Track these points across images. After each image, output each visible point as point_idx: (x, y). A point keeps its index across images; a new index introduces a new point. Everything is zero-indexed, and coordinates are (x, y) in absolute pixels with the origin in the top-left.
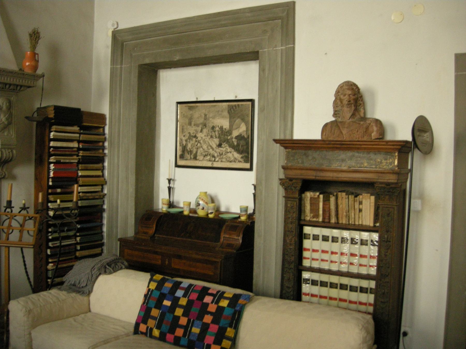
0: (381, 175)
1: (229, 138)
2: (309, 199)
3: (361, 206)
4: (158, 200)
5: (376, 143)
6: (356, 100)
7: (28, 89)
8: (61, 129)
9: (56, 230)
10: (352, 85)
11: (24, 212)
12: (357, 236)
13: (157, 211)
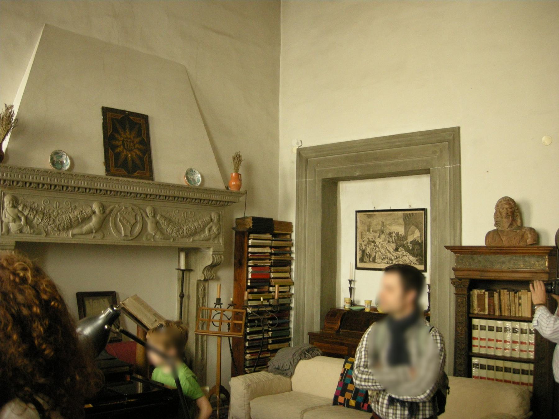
0: (536, 274)
1: (405, 242)
2: (476, 296)
3: (520, 301)
4: (340, 299)
5: (529, 248)
6: (513, 213)
7: (234, 203)
8: (257, 237)
10: (508, 200)
12: (517, 326)
13: (339, 308)
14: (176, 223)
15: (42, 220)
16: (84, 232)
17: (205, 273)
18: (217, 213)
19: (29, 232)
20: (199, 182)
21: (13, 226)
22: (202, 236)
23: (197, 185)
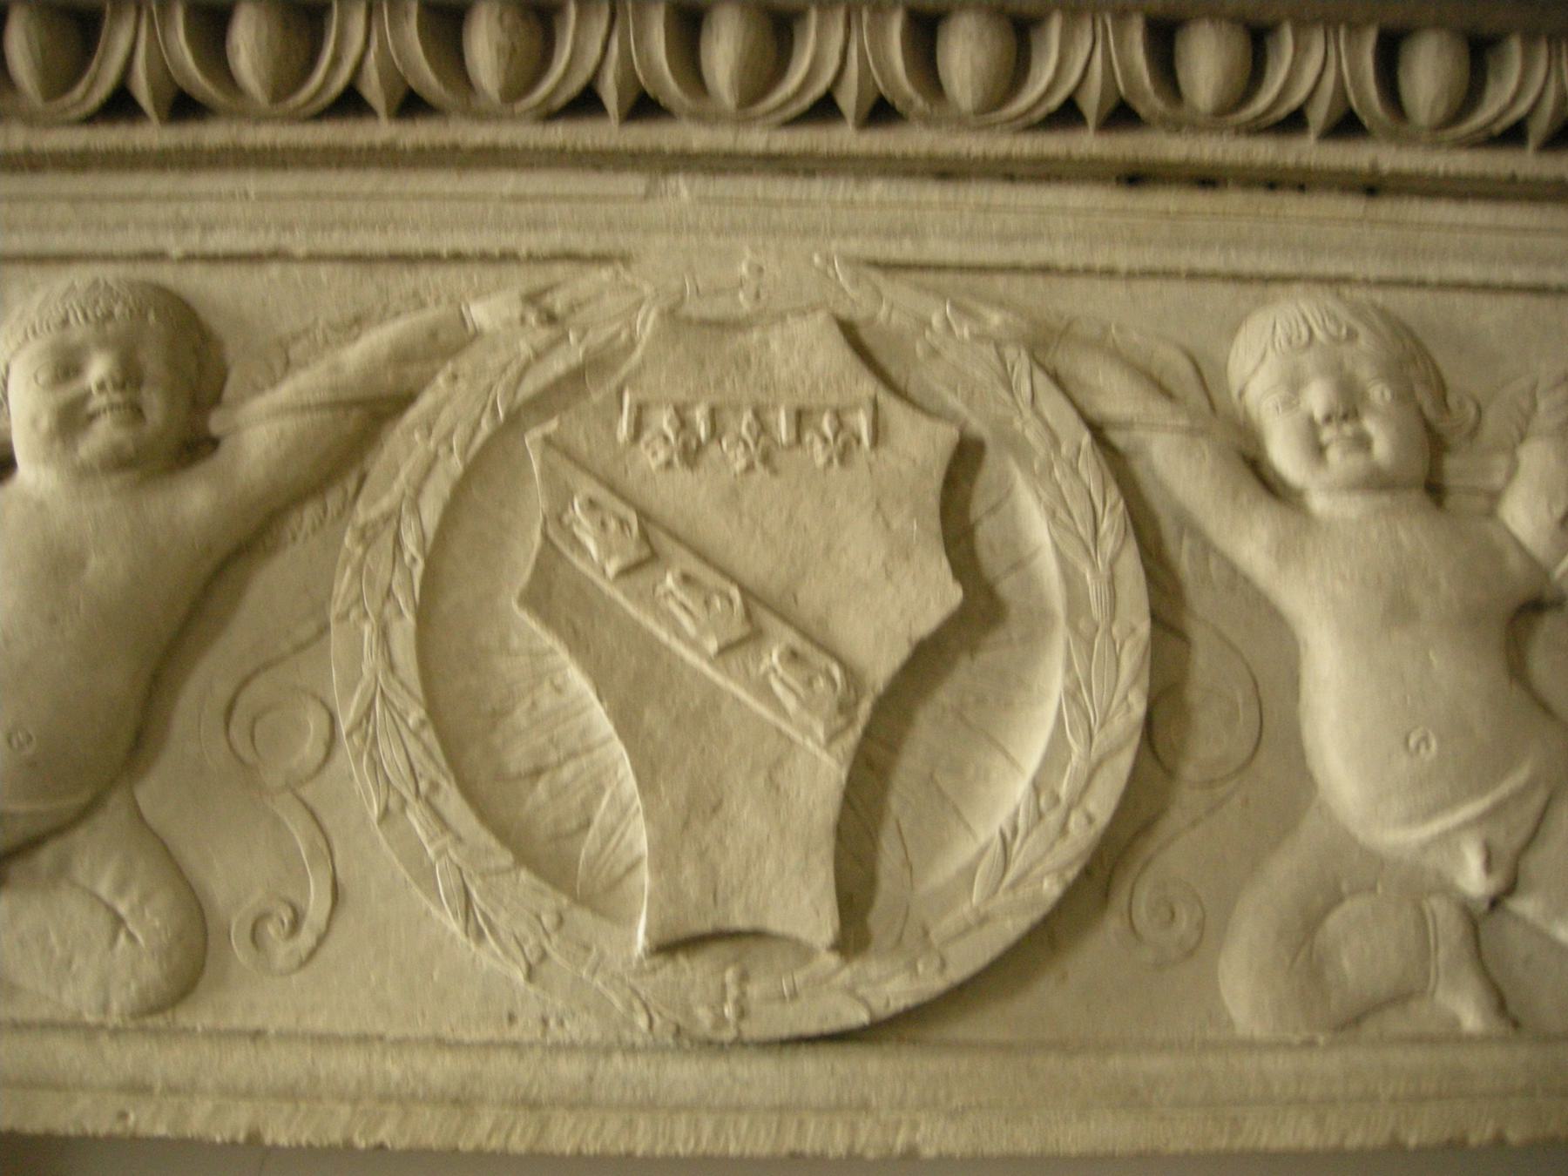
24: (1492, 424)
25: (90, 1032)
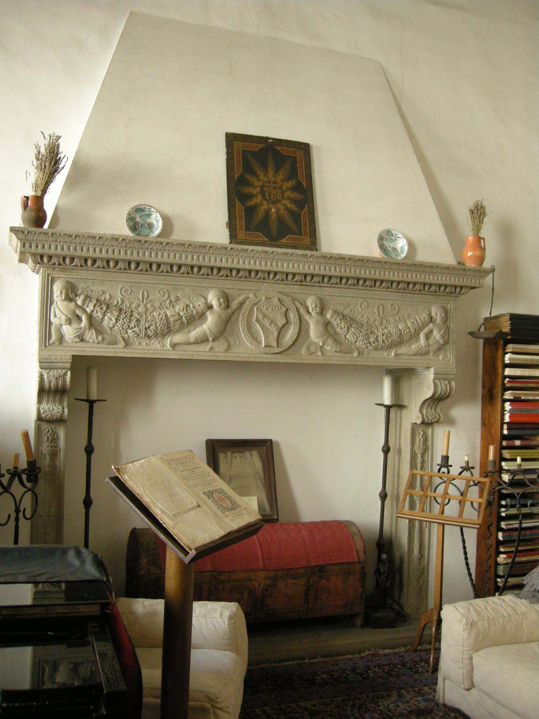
9: (513, 502)
11: (466, 474)
14: (363, 325)
15: (117, 320)
16: (192, 340)
17: (424, 412)
18: (443, 307)
19: (96, 341)
20: (403, 254)
21: (69, 331)
22: (414, 347)
23: (400, 258)
24: (327, 307)
25: (221, 352)
